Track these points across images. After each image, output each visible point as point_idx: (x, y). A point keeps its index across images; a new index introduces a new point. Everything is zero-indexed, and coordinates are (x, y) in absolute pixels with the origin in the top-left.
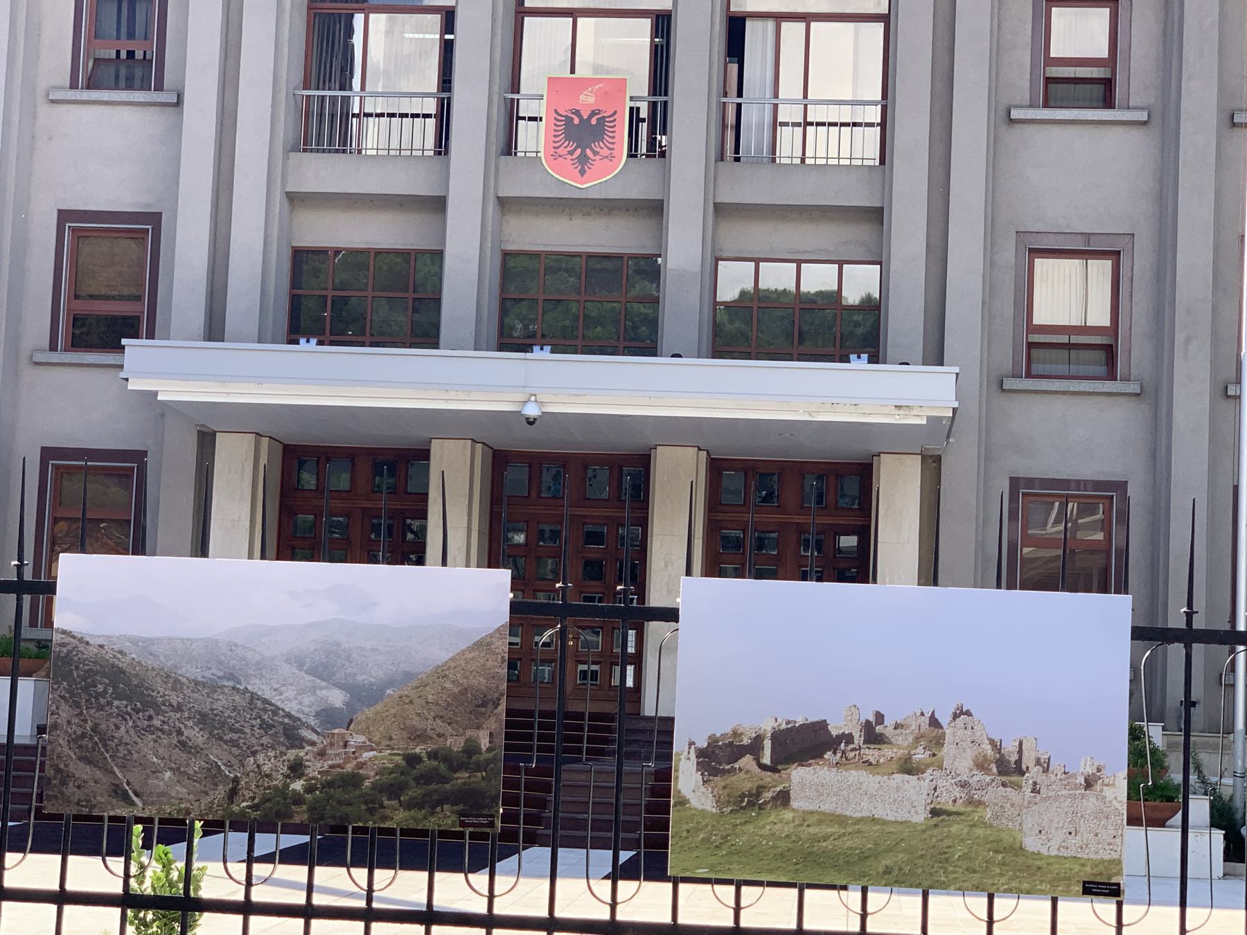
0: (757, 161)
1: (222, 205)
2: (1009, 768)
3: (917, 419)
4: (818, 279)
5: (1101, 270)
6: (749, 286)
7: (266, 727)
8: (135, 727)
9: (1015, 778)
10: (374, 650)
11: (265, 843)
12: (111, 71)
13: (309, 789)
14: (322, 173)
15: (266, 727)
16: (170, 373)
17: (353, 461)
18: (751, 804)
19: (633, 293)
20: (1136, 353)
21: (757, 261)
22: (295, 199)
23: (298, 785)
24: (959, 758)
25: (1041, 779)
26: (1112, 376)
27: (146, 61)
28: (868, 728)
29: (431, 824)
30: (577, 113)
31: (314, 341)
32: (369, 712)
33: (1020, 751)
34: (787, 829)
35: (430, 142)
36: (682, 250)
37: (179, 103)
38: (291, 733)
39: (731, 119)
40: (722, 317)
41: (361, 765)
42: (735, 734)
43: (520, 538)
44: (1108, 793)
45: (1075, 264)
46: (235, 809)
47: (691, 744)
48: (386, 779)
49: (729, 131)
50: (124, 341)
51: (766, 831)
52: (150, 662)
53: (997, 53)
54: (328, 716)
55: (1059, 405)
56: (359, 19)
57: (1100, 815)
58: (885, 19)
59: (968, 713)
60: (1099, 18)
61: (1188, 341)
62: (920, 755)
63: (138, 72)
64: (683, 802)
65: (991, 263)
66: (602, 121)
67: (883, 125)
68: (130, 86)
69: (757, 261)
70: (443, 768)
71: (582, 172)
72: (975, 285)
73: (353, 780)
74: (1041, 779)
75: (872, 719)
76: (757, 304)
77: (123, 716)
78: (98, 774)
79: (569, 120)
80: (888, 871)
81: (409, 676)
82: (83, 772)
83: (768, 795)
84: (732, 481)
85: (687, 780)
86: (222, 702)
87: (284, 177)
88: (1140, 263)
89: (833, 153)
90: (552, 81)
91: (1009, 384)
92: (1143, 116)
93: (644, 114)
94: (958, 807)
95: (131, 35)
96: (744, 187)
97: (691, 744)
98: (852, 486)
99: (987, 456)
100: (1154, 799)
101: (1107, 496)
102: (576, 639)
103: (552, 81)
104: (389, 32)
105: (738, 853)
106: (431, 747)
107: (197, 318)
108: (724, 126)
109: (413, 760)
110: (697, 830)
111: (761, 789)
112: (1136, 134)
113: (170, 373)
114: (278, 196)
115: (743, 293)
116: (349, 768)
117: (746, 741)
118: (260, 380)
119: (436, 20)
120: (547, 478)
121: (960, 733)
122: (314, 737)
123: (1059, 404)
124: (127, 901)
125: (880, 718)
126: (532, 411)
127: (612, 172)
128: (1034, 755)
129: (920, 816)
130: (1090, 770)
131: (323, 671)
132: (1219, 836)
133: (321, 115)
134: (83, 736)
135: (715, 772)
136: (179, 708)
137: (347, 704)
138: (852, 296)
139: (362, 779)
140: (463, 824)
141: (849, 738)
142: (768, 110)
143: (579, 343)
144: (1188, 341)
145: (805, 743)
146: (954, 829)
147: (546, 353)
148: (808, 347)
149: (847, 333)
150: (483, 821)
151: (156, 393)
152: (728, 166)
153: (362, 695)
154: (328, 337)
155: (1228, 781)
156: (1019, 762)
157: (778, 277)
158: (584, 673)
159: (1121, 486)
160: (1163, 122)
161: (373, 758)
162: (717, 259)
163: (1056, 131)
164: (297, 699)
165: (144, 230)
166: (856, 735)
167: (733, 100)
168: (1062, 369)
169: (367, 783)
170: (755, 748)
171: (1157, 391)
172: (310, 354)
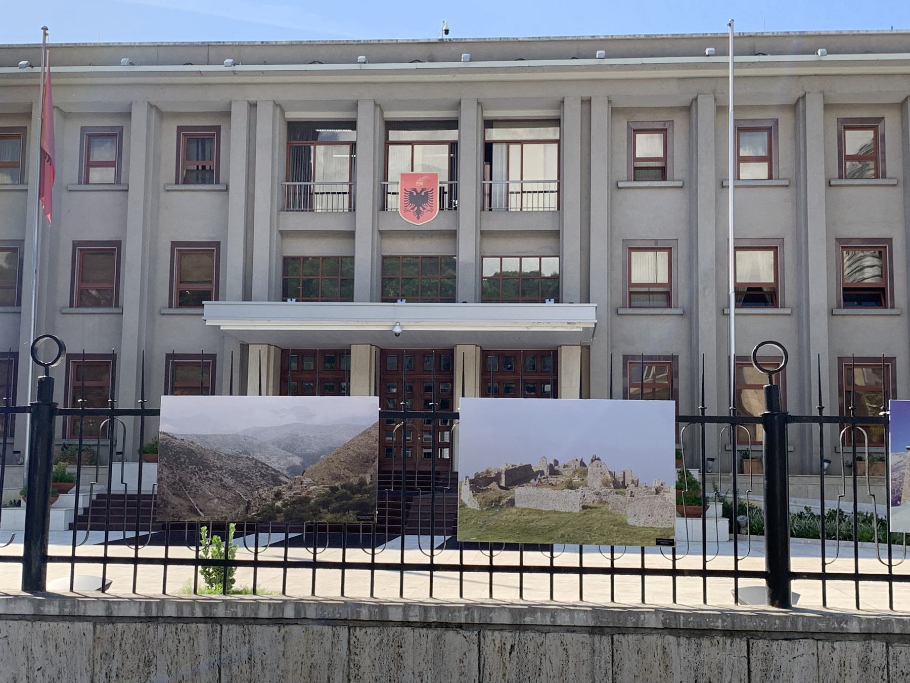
0: (499, 210)
1: (249, 236)
2: (619, 485)
4: (530, 265)
5: (663, 256)
6: (499, 271)
7: (263, 476)
8: (200, 478)
9: (622, 490)
10: (315, 437)
11: (114, 535)
12: (194, 175)
13: (285, 505)
14: (296, 221)
15: (263, 476)
16: (227, 317)
17: (314, 356)
18: (496, 506)
19: (445, 275)
20: (681, 296)
21: (501, 257)
22: (284, 234)
23: (279, 504)
24: (595, 481)
25: (634, 489)
26: (669, 306)
27: (211, 171)
28: (551, 467)
29: (344, 520)
30: (415, 190)
31: (294, 300)
32: (312, 467)
33: (624, 477)
34: (514, 517)
35: (347, 206)
36: (466, 253)
37: (227, 189)
38: (275, 479)
39: (487, 191)
40: (486, 284)
41: (309, 493)
42: (488, 472)
43: (395, 390)
44: (666, 495)
45: (651, 254)
46: (249, 516)
47: (467, 477)
48: (321, 499)
49: (487, 195)
50: (204, 302)
51: (504, 519)
52: (206, 447)
53: (611, 155)
54: (293, 470)
55: (644, 321)
56: (312, 147)
57: (664, 506)
58: (558, 142)
59: (599, 459)
60: (658, 139)
61: (705, 289)
62: (576, 480)
63: (207, 176)
64: (464, 505)
65: (611, 255)
66: (427, 193)
67: (558, 191)
68: (204, 182)
69: (501, 257)
70: (349, 492)
71: (418, 218)
72: (604, 266)
73: (306, 500)
74: (634, 489)
75: (552, 463)
76: (502, 278)
77: (193, 473)
78: (182, 502)
79: (411, 193)
80: (563, 536)
81: (331, 449)
82: (175, 500)
83: (504, 501)
84: (492, 360)
85: (465, 494)
86: (241, 465)
88: (681, 253)
89: (535, 205)
90: (403, 175)
91: (620, 311)
93: (446, 190)
94: (595, 505)
95: (204, 158)
96: (494, 223)
97: (467, 477)
98: (549, 362)
99: (612, 346)
100: (691, 502)
102: (421, 436)
103: (403, 175)
104: (325, 154)
105: (490, 529)
106: (342, 483)
107: (239, 290)
108: (484, 194)
109: (334, 489)
110: (471, 519)
111: (500, 498)
113: (227, 317)
114: (275, 233)
115: (496, 274)
116: (303, 494)
117: (493, 475)
118: (269, 319)
119: (347, 148)
120: (406, 362)
121: (595, 469)
122: (286, 480)
124: (196, 562)
125: (556, 462)
126: (397, 330)
127: (432, 217)
128: (630, 479)
129: (577, 509)
130: (657, 485)
131: (290, 447)
133: (295, 194)
134: (175, 483)
135: (479, 491)
136: (221, 468)
137: (302, 463)
138: (547, 273)
139: (310, 499)
140: (359, 520)
141: (542, 473)
142: (504, 186)
143: (419, 298)
144: (705, 289)
145: (521, 475)
146: (593, 515)
147: (404, 303)
148: (527, 297)
149: (543, 289)
150: (368, 517)
151: (219, 326)
152: (486, 213)
153: (310, 459)
154: (301, 298)
156: (624, 482)
157: (511, 265)
158: (425, 454)
159: (674, 358)
160: (690, 186)
161: (315, 489)
162: (483, 257)
163: (640, 191)
164: (278, 462)
165: (212, 251)
166: (545, 471)
167: (488, 182)
168: (646, 303)
169: (312, 501)
170: (497, 478)
171: (691, 314)
172: (388, 308)
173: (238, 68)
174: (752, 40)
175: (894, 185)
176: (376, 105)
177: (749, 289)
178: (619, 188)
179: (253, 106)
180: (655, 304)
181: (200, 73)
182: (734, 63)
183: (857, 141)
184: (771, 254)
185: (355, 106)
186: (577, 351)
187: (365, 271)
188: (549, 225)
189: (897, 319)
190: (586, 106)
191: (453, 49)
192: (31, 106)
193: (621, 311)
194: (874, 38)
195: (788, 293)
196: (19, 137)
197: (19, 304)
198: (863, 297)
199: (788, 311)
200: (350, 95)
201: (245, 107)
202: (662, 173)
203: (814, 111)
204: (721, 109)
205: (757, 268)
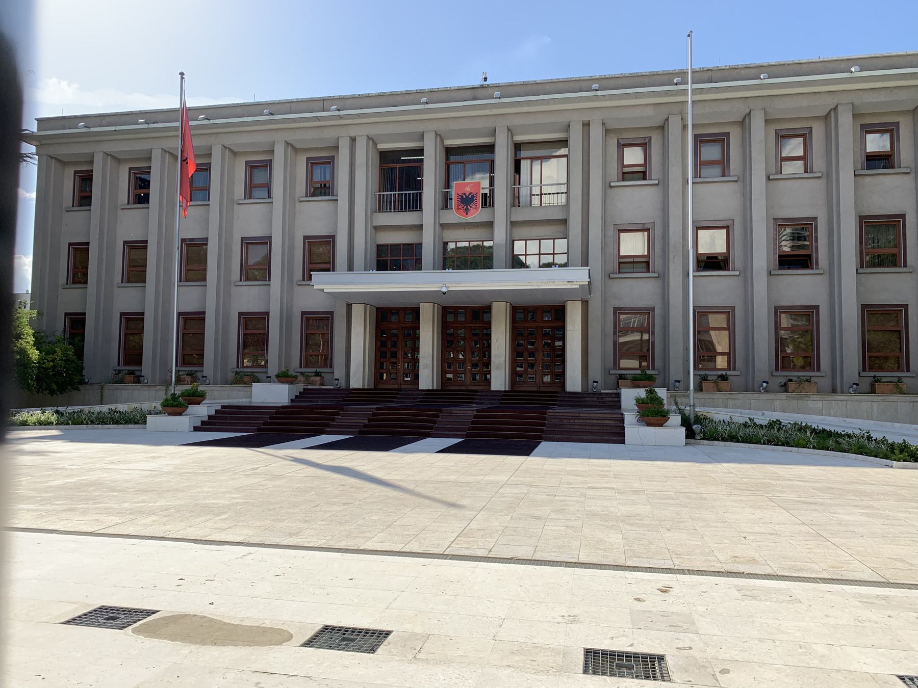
0: (525, 206)
3: (575, 286)
12: (319, 191)
20: (656, 263)
21: (526, 240)
22: (377, 228)
26: (648, 271)
49: (515, 200)
65: (604, 236)
68: (325, 195)
69: (526, 240)
87: (372, 221)
88: (657, 232)
92: (656, 182)
96: (520, 215)
99: (605, 301)
101: (648, 312)
112: (654, 189)
118: (386, 283)
123: (630, 282)
126: (444, 290)
132: (683, 429)
144: (674, 257)
147: (451, 270)
155: (688, 408)
159: (653, 309)
160: (663, 184)
163: (627, 189)
165: (329, 241)
173: (341, 113)
174: (710, 73)
175: (819, 177)
176: (437, 134)
177: (708, 258)
178: (611, 187)
179: (353, 140)
180: (638, 270)
181: (317, 119)
182: (693, 90)
183: (634, 156)
184: (725, 231)
185: (421, 137)
186: (579, 305)
187: (428, 252)
188: (560, 216)
189: (820, 277)
190: (586, 128)
191: (490, 91)
192: (210, 148)
193: (612, 276)
194: (805, 66)
195: (737, 260)
196: (329, 163)
197: (269, 280)
198: (796, 260)
199: (738, 273)
200: (419, 128)
201: (580, 128)
202: (643, 175)
203: (757, 125)
204: (685, 127)
205: (713, 242)
